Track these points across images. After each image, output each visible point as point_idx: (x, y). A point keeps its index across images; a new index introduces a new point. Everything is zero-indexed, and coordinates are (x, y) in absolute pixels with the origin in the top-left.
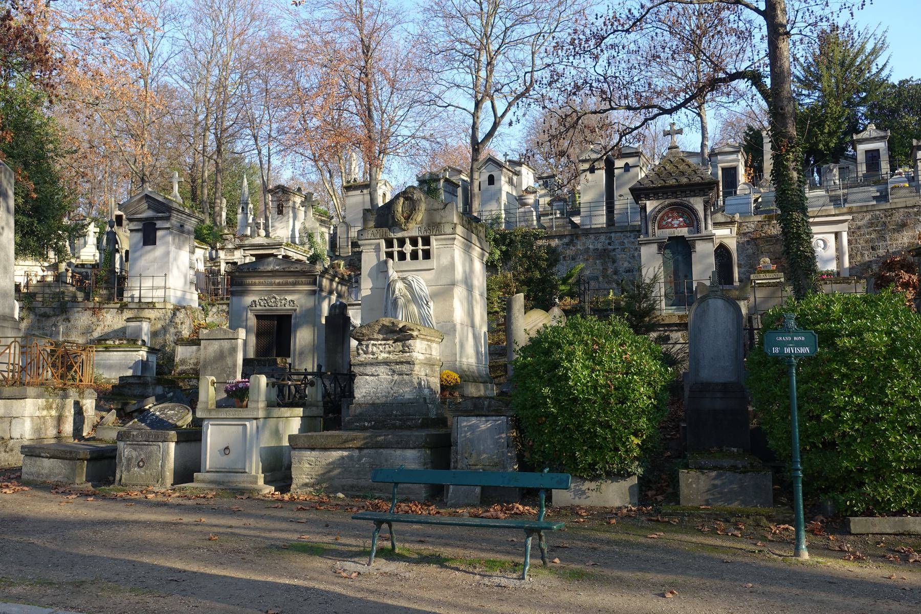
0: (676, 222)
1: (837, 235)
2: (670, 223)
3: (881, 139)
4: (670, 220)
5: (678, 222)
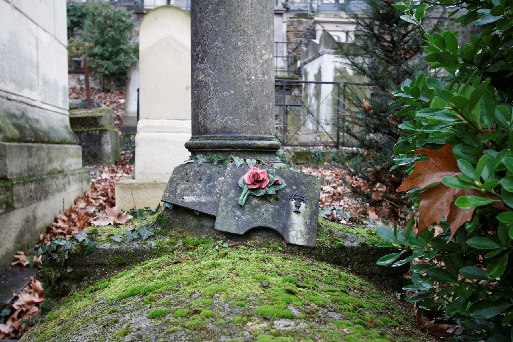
1: (347, 33)
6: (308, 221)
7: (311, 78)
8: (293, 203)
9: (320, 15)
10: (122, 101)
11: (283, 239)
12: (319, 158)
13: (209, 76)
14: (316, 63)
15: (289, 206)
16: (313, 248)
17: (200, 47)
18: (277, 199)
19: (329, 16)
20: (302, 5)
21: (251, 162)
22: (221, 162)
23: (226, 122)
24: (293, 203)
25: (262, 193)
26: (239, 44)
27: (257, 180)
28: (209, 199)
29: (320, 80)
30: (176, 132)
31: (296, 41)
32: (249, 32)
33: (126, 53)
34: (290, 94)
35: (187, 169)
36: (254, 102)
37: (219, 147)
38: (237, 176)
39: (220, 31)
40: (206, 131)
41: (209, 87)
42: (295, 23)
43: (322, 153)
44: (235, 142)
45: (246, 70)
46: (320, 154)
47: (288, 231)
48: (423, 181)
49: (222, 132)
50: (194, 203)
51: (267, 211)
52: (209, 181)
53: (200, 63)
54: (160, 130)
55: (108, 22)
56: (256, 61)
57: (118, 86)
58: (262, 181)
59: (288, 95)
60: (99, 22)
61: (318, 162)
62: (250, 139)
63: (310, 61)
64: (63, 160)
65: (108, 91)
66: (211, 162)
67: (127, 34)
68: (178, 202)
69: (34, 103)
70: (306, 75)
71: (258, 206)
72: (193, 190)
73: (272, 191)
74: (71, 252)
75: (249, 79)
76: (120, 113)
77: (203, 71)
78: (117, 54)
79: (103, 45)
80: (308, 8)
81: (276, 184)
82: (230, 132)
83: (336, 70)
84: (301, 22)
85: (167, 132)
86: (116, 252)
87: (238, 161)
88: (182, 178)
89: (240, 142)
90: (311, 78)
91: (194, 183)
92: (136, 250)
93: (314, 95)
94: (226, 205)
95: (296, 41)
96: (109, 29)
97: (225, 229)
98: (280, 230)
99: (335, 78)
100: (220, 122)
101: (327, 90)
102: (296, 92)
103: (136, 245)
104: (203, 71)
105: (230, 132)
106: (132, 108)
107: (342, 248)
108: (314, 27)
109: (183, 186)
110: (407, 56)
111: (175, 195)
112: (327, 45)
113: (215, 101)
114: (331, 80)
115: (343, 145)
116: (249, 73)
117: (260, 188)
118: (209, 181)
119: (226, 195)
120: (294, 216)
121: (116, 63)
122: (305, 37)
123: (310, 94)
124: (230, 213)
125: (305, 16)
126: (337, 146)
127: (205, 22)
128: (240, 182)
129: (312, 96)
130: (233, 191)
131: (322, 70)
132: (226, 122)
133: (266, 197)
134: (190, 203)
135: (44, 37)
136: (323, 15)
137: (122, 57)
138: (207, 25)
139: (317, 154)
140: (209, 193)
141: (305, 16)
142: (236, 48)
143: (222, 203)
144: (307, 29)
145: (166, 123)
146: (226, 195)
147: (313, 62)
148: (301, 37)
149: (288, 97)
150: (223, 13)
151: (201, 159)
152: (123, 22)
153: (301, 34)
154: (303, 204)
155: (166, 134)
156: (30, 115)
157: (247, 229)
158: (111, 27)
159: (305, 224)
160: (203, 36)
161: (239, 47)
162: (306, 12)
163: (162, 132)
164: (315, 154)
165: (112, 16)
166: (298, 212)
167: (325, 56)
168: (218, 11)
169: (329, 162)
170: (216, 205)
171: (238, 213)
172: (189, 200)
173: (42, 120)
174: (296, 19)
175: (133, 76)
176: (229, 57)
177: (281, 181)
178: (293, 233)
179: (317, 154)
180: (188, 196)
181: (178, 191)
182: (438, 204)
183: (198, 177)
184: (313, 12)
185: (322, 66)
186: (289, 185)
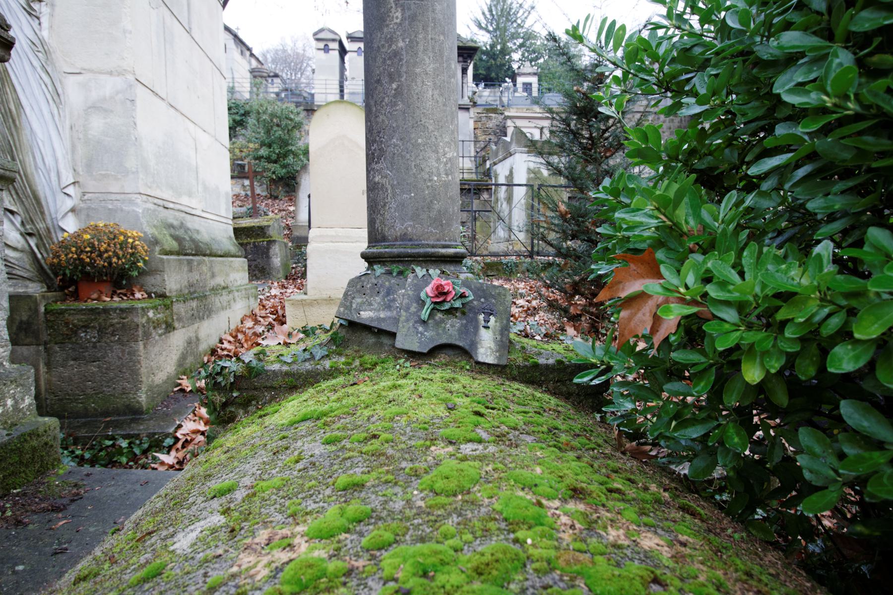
1: (542, 129)
3: (535, 74)
6: (499, 337)
7: (502, 180)
8: (481, 317)
10: (292, 209)
11: (471, 357)
13: (386, 177)
15: (477, 321)
18: (464, 313)
20: (490, 98)
21: (434, 272)
22: (401, 273)
23: (406, 228)
24: (481, 317)
25: (447, 306)
26: (420, 141)
27: (441, 292)
28: (389, 314)
32: (431, 128)
33: (295, 155)
35: (363, 282)
36: (437, 206)
37: (399, 256)
38: (418, 288)
39: (398, 127)
40: (384, 239)
41: (387, 189)
45: (427, 170)
47: (477, 348)
48: (623, 289)
49: (402, 240)
50: (372, 319)
51: (453, 326)
52: (388, 294)
55: (275, 120)
56: (438, 160)
57: (287, 192)
58: (446, 294)
60: (264, 120)
62: (433, 246)
63: (501, 161)
64: (227, 275)
65: (276, 198)
66: (389, 273)
67: (296, 133)
68: (355, 318)
69: (193, 212)
71: (442, 321)
73: (458, 304)
75: (430, 181)
76: (290, 222)
77: (379, 171)
78: (285, 156)
79: (270, 146)
80: (498, 103)
81: (463, 296)
82: (411, 240)
84: (490, 118)
86: (287, 374)
87: (420, 271)
88: (358, 291)
90: (502, 180)
91: (372, 296)
92: (308, 372)
93: (505, 199)
94: (407, 320)
96: (275, 128)
98: (467, 348)
99: (529, 179)
100: (399, 228)
101: (520, 193)
102: (485, 196)
104: (379, 171)
105: (411, 240)
106: (303, 217)
107: (536, 366)
109: (359, 300)
112: (518, 143)
113: (393, 205)
115: (538, 254)
116: (431, 174)
118: (388, 294)
119: (407, 309)
120: (483, 331)
121: (284, 166)
124: (411, 330)
125: (495, 111)
126: (531, 256)
128: (423, 295)
130: (415, 305)
134: (367, 319)
135: (204, 138)
137: (290, 159)
140: (389, 307)
141: (495, 111)
142: (416, 145)
146: (407, 309)
149: (476, 202)
150: (400, 106)
151: (379, 270)
152: (291, 120)
153: (490, 131)
154: (492, 319)
156: (189, 225)
157: (431, 346)
158: (278, 125)
159: (495, 340)
160: (379, 132)
161: (419, 145)
165: (279, 113)
167: (517, 155)
168: (395, 104)
169: (523, 273)
170: (396, 320)
171: (421, 329)
172: (366, 315)
173: (202, 230)
175: (303, 180)
176: (408, 156)
177: (468, 292)
178: (481, 351)
180: (365, 310)
181: (354, 306)
183: (376, 289)
186: (477, 297)
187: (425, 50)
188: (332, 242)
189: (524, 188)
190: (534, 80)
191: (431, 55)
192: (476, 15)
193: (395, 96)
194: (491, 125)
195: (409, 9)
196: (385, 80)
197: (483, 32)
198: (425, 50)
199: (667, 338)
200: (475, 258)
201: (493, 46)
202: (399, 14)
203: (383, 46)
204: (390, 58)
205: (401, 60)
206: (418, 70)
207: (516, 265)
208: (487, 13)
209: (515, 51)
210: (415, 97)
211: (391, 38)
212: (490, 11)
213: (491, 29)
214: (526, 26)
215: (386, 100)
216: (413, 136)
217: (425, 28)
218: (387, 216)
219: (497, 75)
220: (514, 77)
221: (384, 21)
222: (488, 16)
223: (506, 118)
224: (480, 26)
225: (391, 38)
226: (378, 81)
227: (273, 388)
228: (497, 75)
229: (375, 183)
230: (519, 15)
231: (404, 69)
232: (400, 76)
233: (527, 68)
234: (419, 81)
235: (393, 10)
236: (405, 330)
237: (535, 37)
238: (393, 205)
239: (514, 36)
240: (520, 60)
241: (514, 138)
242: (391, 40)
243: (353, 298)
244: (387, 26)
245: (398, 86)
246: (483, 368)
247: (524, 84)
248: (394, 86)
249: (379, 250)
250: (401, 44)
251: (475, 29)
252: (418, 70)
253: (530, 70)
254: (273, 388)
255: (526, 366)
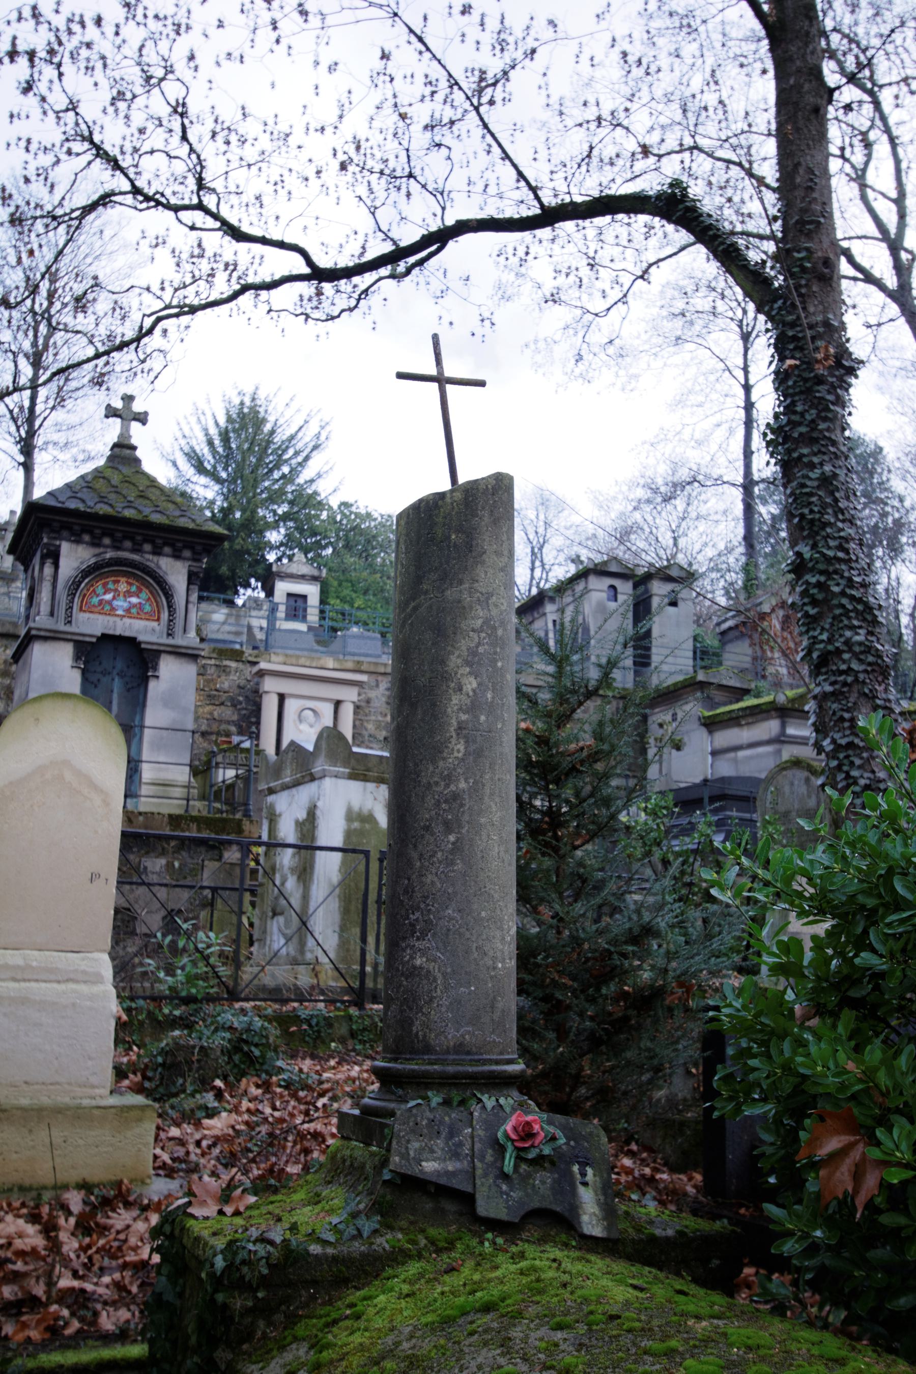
0: (120, 603)
1: (338, 704)
2: (109, 603)
3: (314, 579)
4: (108, 597)
5: (126, 605)
6: (602, 1198)
7: (287, 831)
8: (576, 1168)
9: (274, 658)
11: (575, 1230)
12: (319, 1032)
13: (435, 961)
14: (304, 794)
15: (571, 1173)
16: (616, 1242)
17: (417, 914)
18: (553, 1163)
19: (294, 661)
20: (227, 628)
22: (462, 1102)
23: (463, 1036)
24: (576, 1168)
25: (531, 1155)
26: (483, 914)
28: (458, 1165)
29: (313, 838)
30: (59, 982)
31: (211, 714)
32: (496, 896)
34: (220, 858)
35: (416, 1116)
37: (456, 1076)
39: (455, 893)
41: (435, 980)
42: (211, 671)
43: (325, 1018)
44: (480, 1069)
45: (491, 953)
46: (322, 1023)
47: (578, 1216)
48: (821, 1147)
49: (457, 1052)
50: (438, 1173)
51: (543, 1182)
52: (451, 1135)
53: (418, 939)
54: (19, 977)
59: (211, 859)
61: (315, 1040)
62: (497, 1062)
63: (286, 787)
68: (415, 1171)
70: (273, 818)
71: (529, 1175)
72: (432, 1151)
73: (547, 1151)
74: (273, 1261)
75: (495, 968)
80: (244, 638)
81: (554, 1138)
82: (468, 1053)
83: (351, 816)
84: (225, 670)
85: (37, 981)
86: (335, 1259)
88: (413, 1131)
89: (486, 1068)
90: (287, 831)
91: (431, 1139)
92: (362, 1254)
93: (293, 870)
94: (485, 1175)
95: (211, 714)
97: (492, 1214)
98: (566, 1214)
99: (348, 834)
100: (452, 1035)
102: (232, 855)
103: (358, 1247)
105: (468, 1053)
107: (653, 1239)
108: (258, 684)
109: (416, 1145)
110: (577, 843)
111: (408, 1160)
112: (333, 758)
113: (445, 1002)
114: (338, 842)
116: (494, 959)
117: (533, 1146)
118: (451, 1135)
120: (581, 1190)
122: (234, 706)
123: (282, 866)
124: (494, 1189)
125: (237, 655)
126: (360, 1005)
127: (429, 879)
129: (286, 870)
130: (490, 1151)
131: (318, 813)
132: (463, 1036)
133: (539, 1161)
134: (432, 1173)
136: (281, 659)
138: (433, 882)
139: (314, 1022)
141: (237, 655)
143: (479, 1172)
144: (239, 687)
145: (35, 957)
147: (294, 790)
148: (222, 704)
149: (211, 866)
150: (459, 866)
153: (224, 697)
154: (590, 1171)
155: (33, 985)
157: (522, 1213)
159: (598, 1203)
160: (427, 897)
161: (482, 919)
162: (237, 647)
163: (24, 980)
164: (308, 1021)
166: (585, 1184)
167: (328, 782)
168: (452, 863)
169: (342, 1040)
171: (504, 1187)
174: (213, 662)
176: (468, 935)
178: (585, 1218)
179: (314, 1022)
180: (427, 1160)
181: (412, 1153)
182: (838, 1174)
184: (255, 648)
185: (319, 804)
187: (492, 794)
188: (14, 980)
189: (338, 856)
190: (312, 591)
191: (497, 800)
192: (194, 443)
193: (452, 852)
194: (226, 685)
195: (475, 742)
196: (438, 829)
197: (203, 480)
198: (492, 794)
199: (872, 1199)
200: (237, 1005)
201: (226, 512)
202: (461, 747)
203: (437, 783)
204: (446, 801)
205: (462, 805)
206: (483, 820)
207: (329, 1022)
208: (217, 442)
209: (275, 526)
210: (479, 855)
211: (449, 776)
212: (225, 437)
213: (224, 475)
214: (301, 480)
215: (439, 854)
216: (475, 906)
217: (492, 766)
218: (434, 1015)
219: (233, 571)
220: (268, 581)
221: (441, 752)
222: (220, 450)
223: (261, 674)
224: (200, 468)
225: (449, 776)
226: (427, 828)
227: (314, 1283)
228: (233, 571)
229: (414, 967)
230: (286, 457)
231: (466, 817)
232: (460, 826)
233: (300, 564)
234: (484, 834)
235: (453, 741)
236: (485, 1189)
237: (320, 505)
238: (445, 1002)
239: (275, 497)
240: (282, 544)
241: (324, 745)
242: (449, 779)
243: (408, 1141)
244: (444, 759)
245: (458, 839)
246: (590, 1244)
247: (289, 595)
248: (452, 838)
249: (423, 1068)
250: (463, 785)
251: (189, 471)
252: (483, 820)
253: (306, 570)
254: (314, 1283)
255: (641, 1240)
